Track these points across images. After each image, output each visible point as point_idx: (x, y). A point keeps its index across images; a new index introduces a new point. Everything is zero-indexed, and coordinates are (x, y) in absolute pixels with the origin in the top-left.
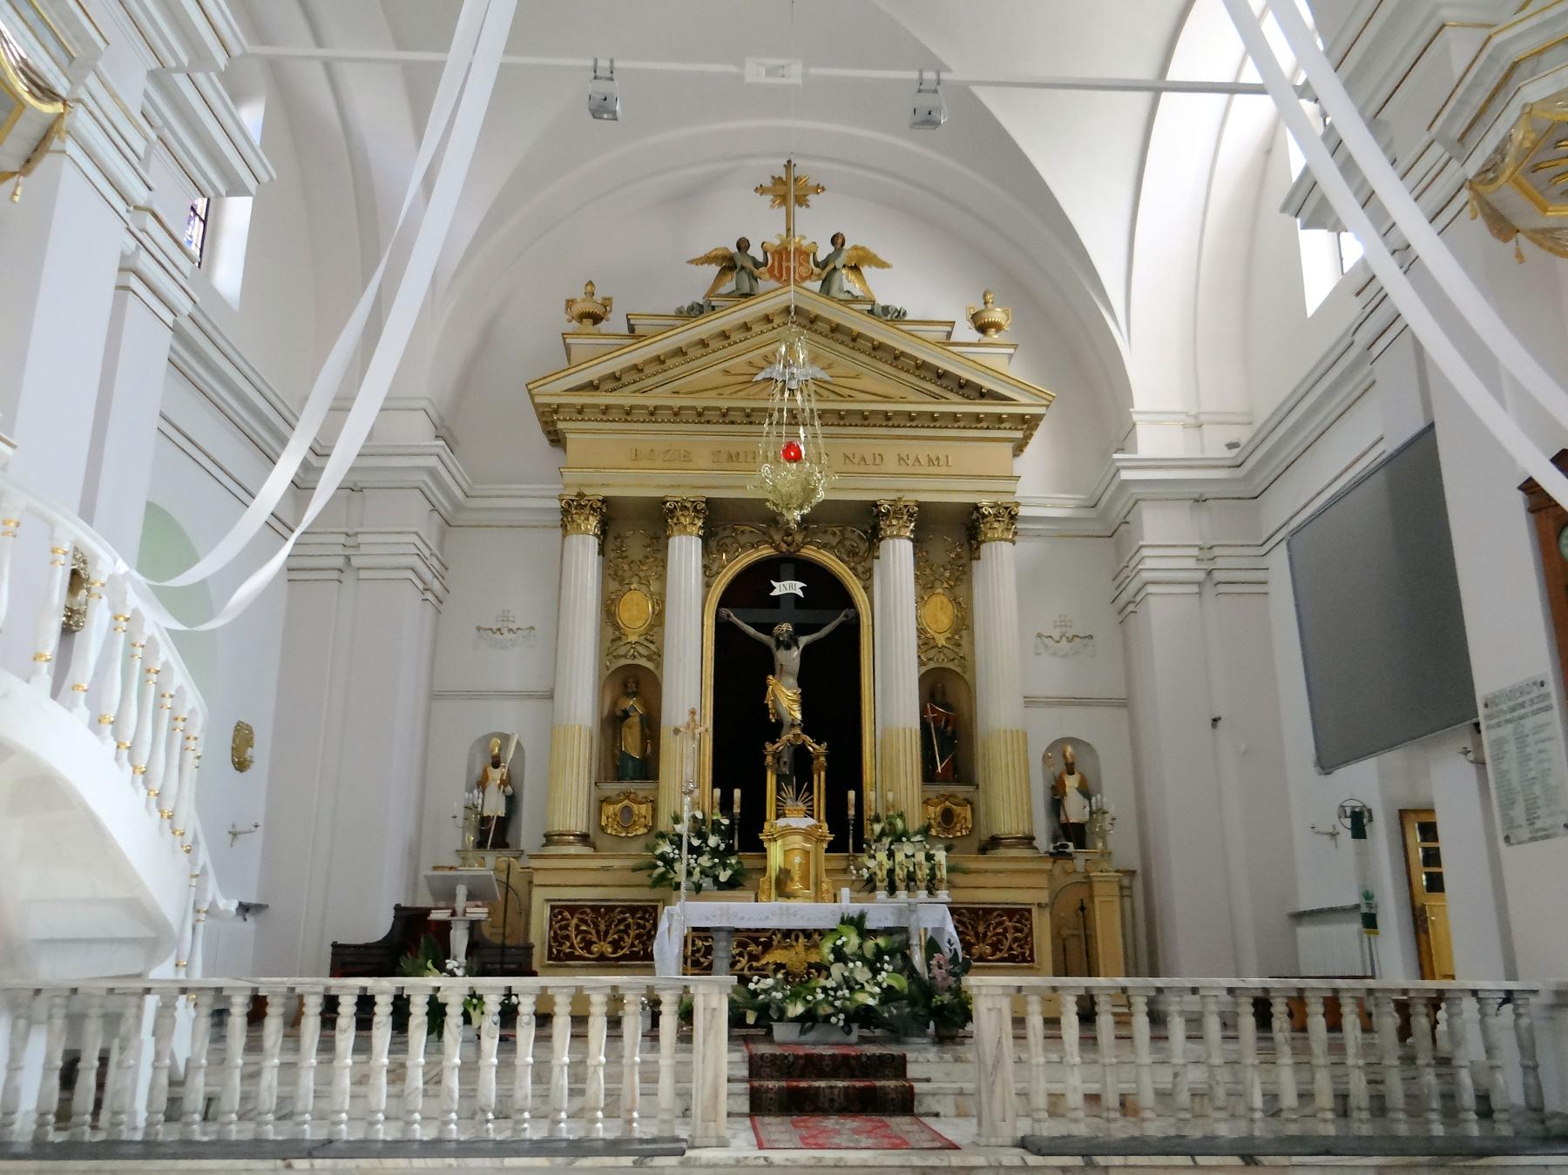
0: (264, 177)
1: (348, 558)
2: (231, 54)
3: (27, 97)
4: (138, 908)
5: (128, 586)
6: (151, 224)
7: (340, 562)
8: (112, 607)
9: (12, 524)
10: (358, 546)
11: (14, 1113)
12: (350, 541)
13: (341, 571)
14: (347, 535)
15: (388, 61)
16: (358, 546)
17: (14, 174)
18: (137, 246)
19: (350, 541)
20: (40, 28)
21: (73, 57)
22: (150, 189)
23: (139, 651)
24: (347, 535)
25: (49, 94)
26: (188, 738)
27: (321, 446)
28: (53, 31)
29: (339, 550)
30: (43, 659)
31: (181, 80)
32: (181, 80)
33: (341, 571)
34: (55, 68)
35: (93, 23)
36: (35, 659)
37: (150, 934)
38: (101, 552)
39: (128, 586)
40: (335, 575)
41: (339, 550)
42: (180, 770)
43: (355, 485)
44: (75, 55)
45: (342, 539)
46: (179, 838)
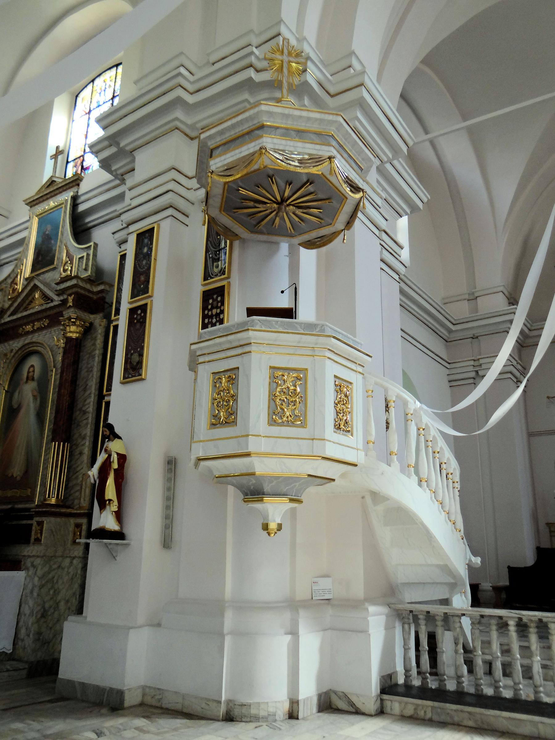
0: (425, 200)
1: (477, 372)
2: (409, 146)
3: (350, 193)
4: (446, 569)
5: (422, 413)
6: (384, 235)
7: (473, 374)
8: (416, 425)
9: (370, 392)
10: (481, 365)
11: (410, 671)
12: (476, 363)
13: (474, 378)
14: (474, 360)
15: (458, 130)
16: (481, 365)
17: (343, 230)
18: (381, 248)
19: (476, 363)
20: (349, 160)
21: (363, 169)
22: (387, 221)
23: (430, 444)
24: (474, 360)
25: (356, 189)
26: (454, 482)
27: (455, 320)
28: (355, 160)
29: (471, 368)
30: (394, 454)
31: (388, 166)
32: (388, 166)
33: (474, 378)
34: (357, 177)
35: (149, 201)
36: (368, 443)
37: (453, 581)
38: (409, 399)
39: (422, 413)
40: (471, 381)
41: (471, 368)
42: (454, 499)
43: (474, 335)
44: (363, 168)
45: (472, 363)
46: (459, 533)
